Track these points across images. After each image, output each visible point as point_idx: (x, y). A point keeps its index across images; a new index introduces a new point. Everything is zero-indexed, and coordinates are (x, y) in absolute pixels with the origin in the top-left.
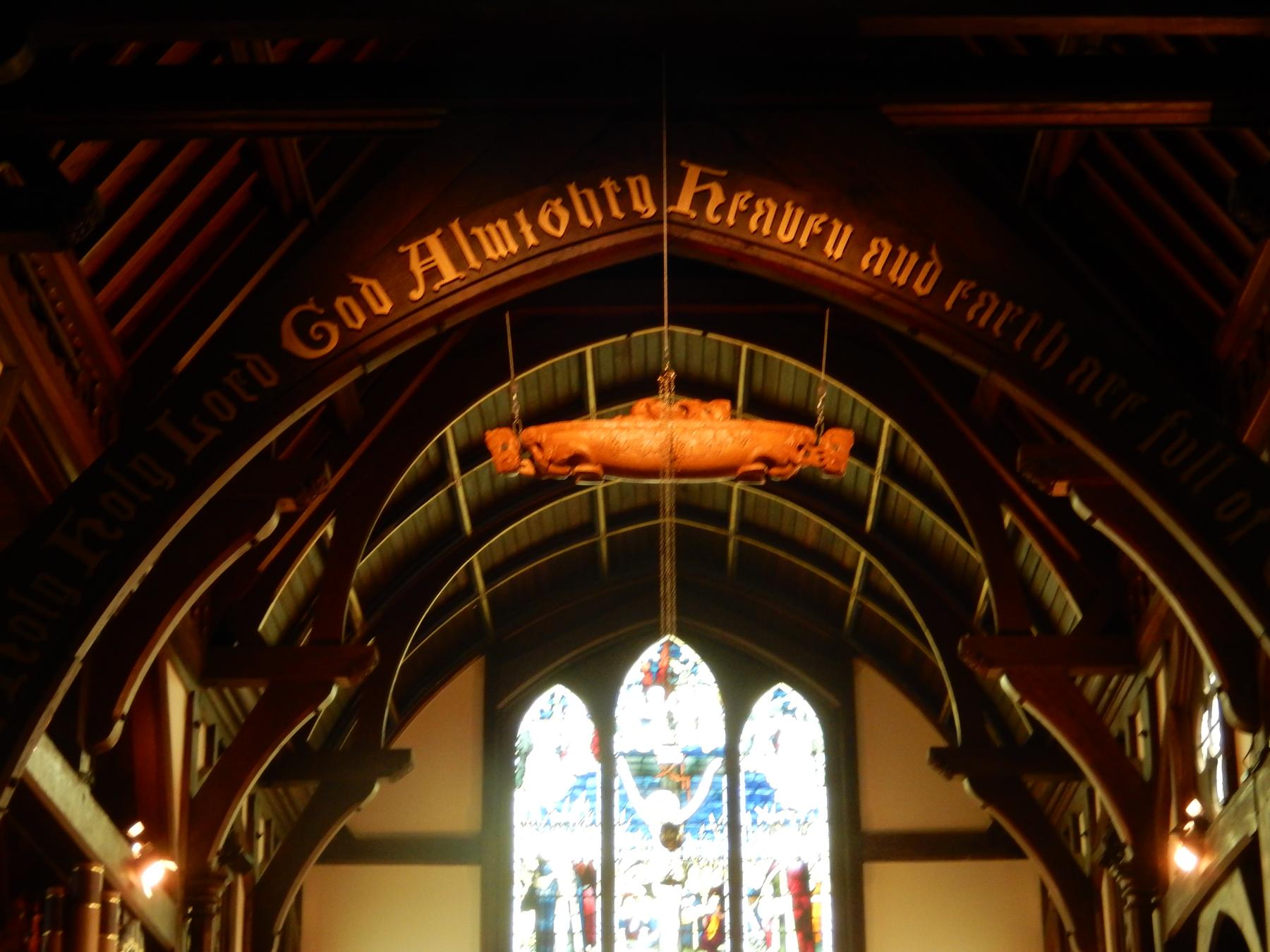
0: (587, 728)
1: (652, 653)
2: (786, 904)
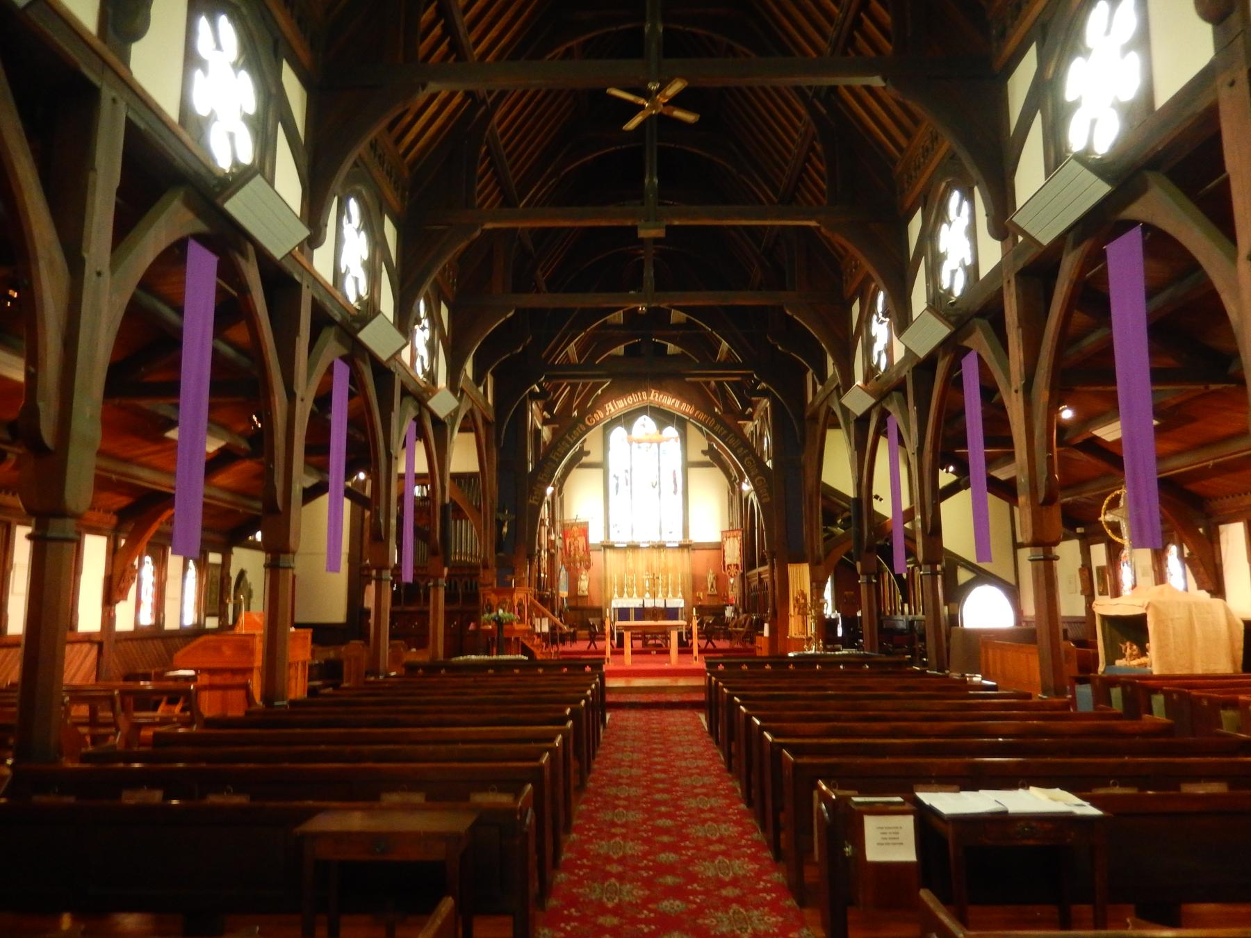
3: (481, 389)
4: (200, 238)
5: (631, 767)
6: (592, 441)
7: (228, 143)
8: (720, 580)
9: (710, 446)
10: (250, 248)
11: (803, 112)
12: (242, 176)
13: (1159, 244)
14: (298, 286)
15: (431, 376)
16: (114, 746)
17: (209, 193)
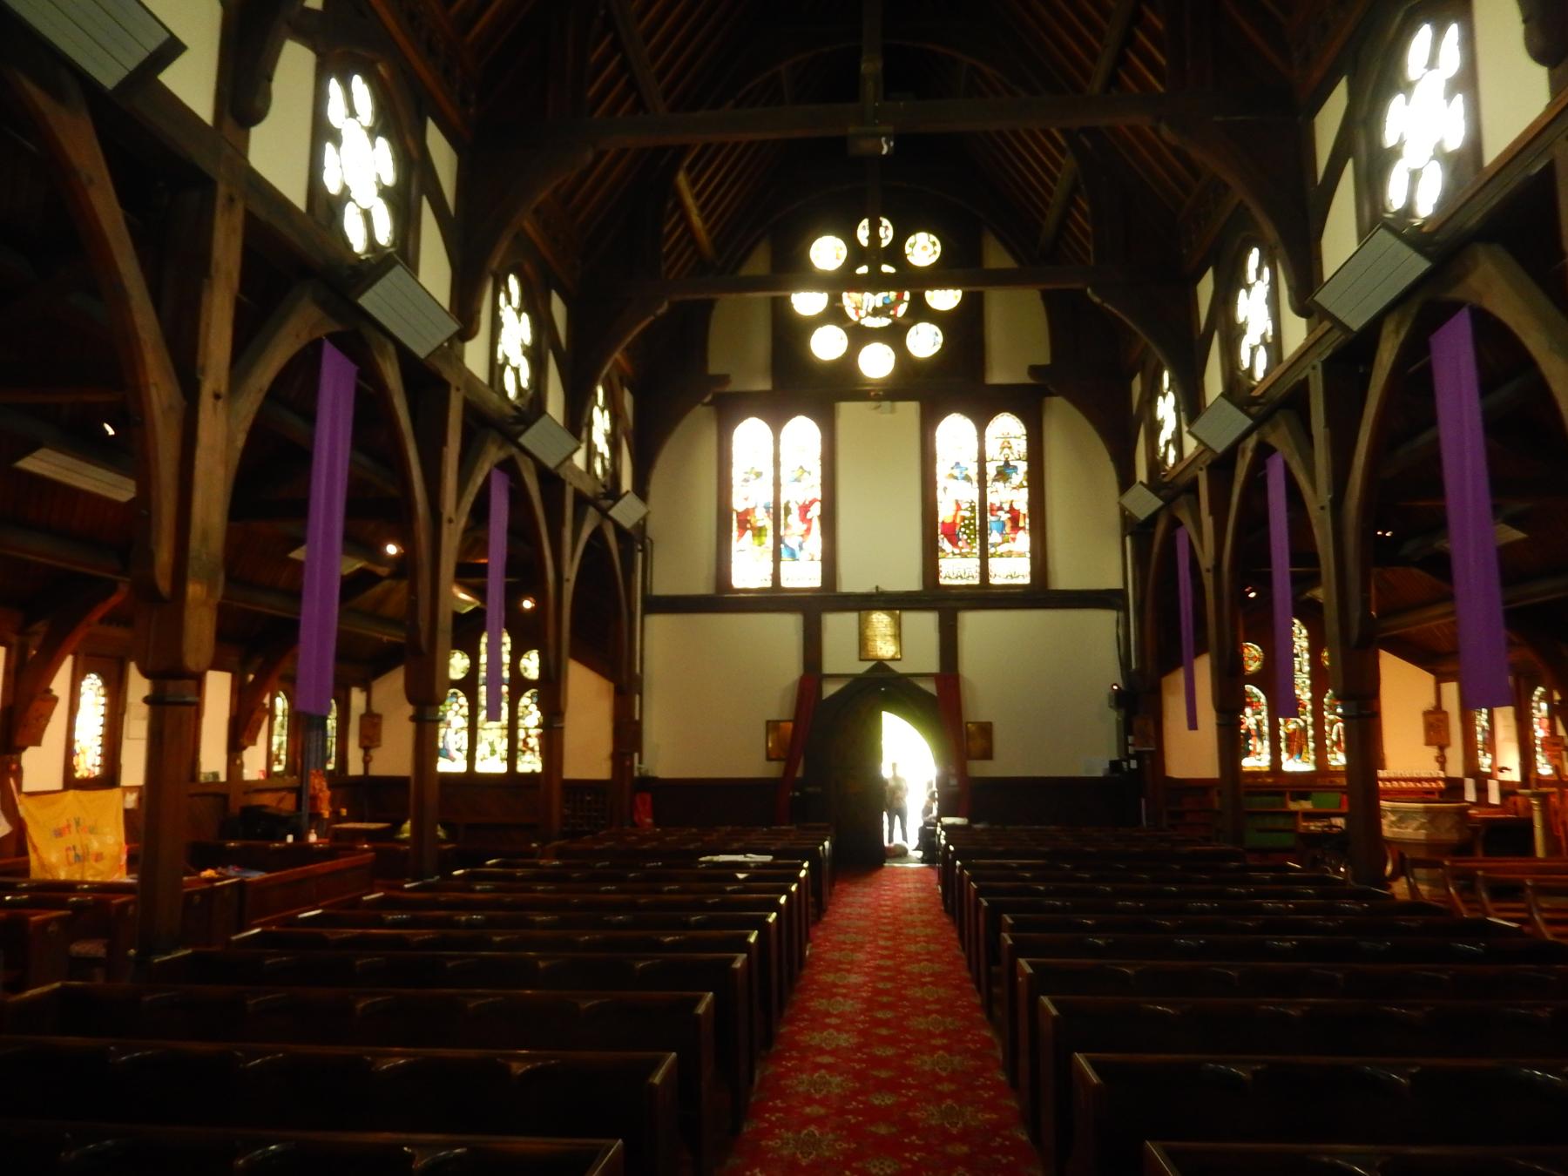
4: (332, 337)
5: (852, 951)
10: (391, 348)
12: (380, 263)
13: (1493, 337)
15: (614, 475)
16: (500, 448)
17: (340, 279)
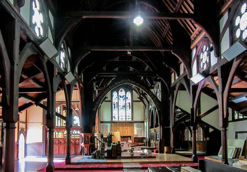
0: (117, 94)
1: (121, 89)
2: (128, 105)
3: (80, 77)
6: (108, 95)
7: (39, 31)
8: (36, 150)
9: (140, 96)
11: (159, 40)
14: (13, 19)
15: (66, 69)
